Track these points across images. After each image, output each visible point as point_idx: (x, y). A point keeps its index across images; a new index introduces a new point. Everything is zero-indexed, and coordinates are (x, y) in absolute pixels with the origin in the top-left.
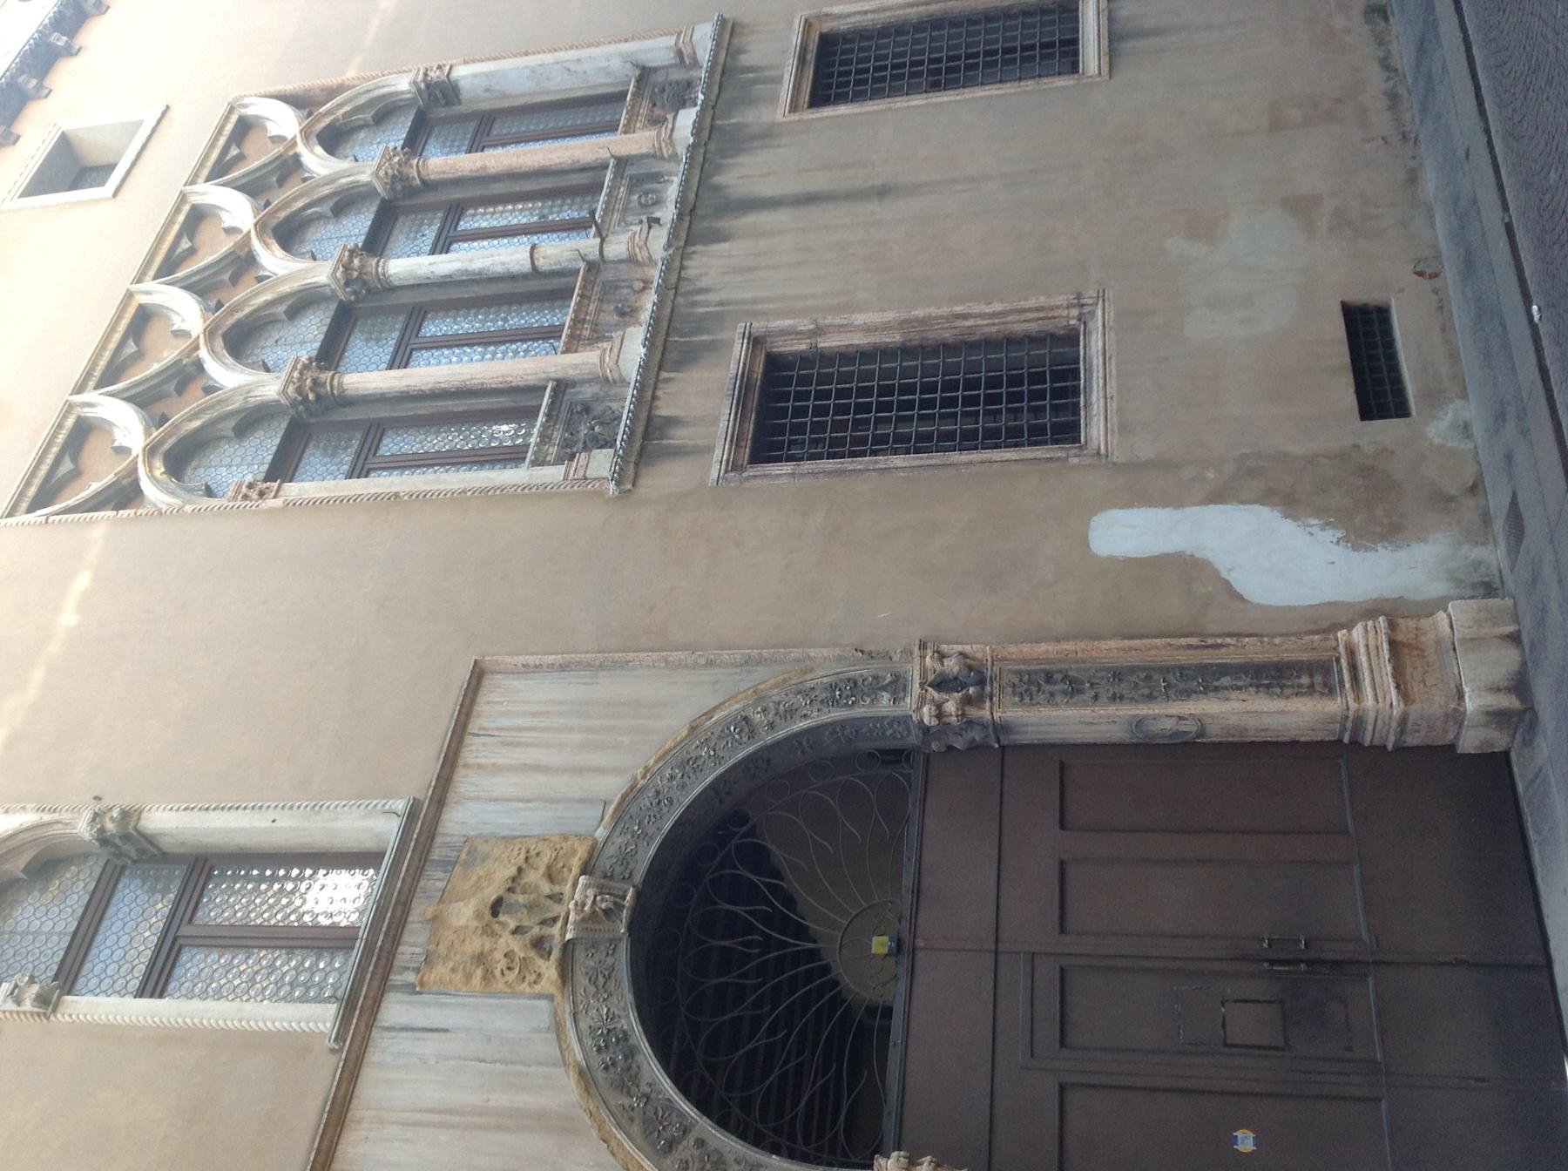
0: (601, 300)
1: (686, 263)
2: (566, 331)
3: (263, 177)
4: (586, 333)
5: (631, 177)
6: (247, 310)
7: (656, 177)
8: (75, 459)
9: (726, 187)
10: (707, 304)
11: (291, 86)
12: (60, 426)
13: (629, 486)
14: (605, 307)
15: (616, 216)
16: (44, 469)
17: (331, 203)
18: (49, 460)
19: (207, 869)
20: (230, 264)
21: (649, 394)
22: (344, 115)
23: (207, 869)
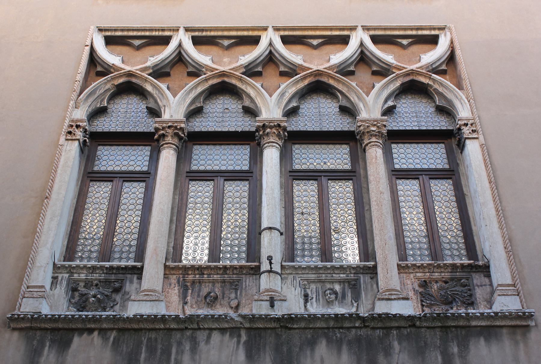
0: (224, 282)
1: (96, 333)
2: (329, 264)
3: (374, 63)
4: (191, 277)
5: (357, 280)
6: (243, 87)
7: (357, 297)
8: (410, 44)
9: (313, 350)
10: (180, 352)
11: (458, 53)
12: (163, 30)
13: (12, 325)
14: (218, 285)
15: (312, 276)
16: (220, 33)
17: (348, 105)
18: (139, 34)
19: (451, 176)
20: (291, 68)
21: (93, 326)
22: (435, 90)
23: (451, 176)
